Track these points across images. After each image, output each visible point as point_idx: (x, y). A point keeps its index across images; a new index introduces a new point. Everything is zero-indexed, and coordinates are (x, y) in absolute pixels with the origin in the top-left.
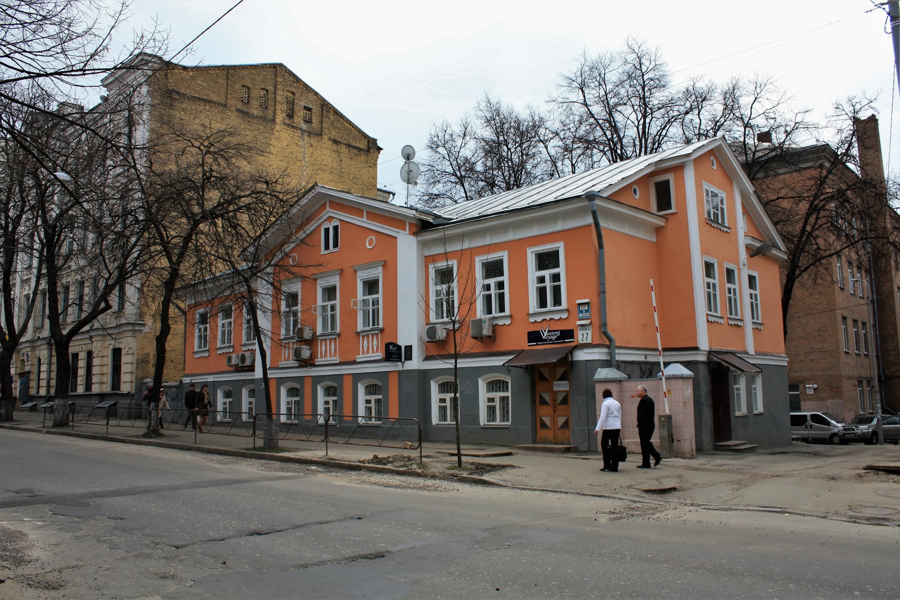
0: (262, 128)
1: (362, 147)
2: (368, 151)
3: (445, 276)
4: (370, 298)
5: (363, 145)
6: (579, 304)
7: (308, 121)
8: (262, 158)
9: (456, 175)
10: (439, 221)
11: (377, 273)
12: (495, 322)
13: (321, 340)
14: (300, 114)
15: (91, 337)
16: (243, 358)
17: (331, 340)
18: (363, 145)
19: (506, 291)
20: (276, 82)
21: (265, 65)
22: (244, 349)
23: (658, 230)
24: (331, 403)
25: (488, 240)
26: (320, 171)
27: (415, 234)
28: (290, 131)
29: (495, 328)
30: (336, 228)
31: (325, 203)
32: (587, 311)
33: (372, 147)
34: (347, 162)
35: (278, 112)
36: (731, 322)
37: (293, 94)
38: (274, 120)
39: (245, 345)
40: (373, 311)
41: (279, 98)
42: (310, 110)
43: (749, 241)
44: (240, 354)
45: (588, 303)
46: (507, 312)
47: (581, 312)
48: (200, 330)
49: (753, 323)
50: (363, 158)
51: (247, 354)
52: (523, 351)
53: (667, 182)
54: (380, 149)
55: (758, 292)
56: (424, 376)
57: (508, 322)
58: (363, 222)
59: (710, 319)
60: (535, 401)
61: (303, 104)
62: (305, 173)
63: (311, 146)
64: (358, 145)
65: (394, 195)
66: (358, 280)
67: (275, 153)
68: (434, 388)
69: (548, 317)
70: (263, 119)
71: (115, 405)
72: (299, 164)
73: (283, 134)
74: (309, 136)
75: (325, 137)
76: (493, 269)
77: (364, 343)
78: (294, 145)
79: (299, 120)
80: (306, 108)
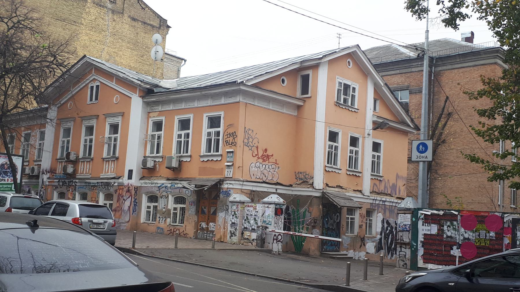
1: (155, 24)
2: (159, 28)
3: (158, 126)
4: (157, 133)
5: (156, 23)
6: (228, 152)
11: (118, 120)
12: (182, 159)
13: (82, 162)
16: (33, 169)
17: (87, 162)
18: (156, 23)
19: (190, 139)
22: (35, 163)
23: (299, 107)
25: (183, 106)
26: (120, 40)
27: (142, 97)
29: (180, 162)
30: (97, 87)
31: (92, 69)
32: (231, 157)
36: (348, 173)
39: (36, 161)
43: (375, 119)
44: (31, 167)
45: (232, 152)
46: (161, 154)
49: (371, 175)
51: (36, 167)
53: (308, 76)
54: (169, 27)
57: (188, 159)
58: (113, 85)
59: (327, 169)
60: (198, 212)
63: (114, 20)
64: (152, 23)
65: (185, 61)
66: (107, 123)
69: (210, 159)
75: (125, 15)
76: (185, 124)
77: (106, 166)
78: (100, 20)
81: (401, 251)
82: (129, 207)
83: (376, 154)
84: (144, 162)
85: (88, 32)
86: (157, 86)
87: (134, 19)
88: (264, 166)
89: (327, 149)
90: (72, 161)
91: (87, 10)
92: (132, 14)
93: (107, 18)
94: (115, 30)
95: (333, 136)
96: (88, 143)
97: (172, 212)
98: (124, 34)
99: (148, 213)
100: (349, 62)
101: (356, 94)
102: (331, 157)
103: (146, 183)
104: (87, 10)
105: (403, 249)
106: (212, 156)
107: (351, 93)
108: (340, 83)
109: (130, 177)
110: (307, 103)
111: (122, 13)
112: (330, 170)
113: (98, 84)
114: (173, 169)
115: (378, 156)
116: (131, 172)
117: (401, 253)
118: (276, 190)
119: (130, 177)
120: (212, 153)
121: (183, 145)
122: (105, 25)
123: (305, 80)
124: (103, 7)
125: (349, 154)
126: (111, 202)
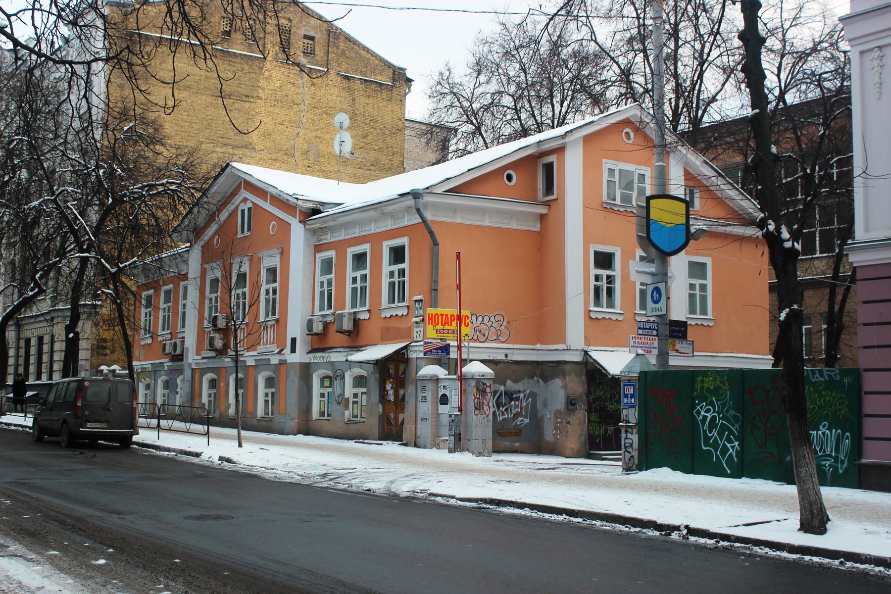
0: (246, 67)
6: (416, 301)
8: (247, 105)
9: (472, 123)
14: (298, 46)
15: (52, 319)
23: (542, 217)
26: (324, 116)
30: (250, 209)
32: (421, 308)
33: (400, 79)
34: (362, 100)
37: (290, 20)
40: (361, 288)
42: (312, 38)
45: (421, 300)
48: (211, 299)
50: (385, 94)
54: (409, 81)
55: (709, 282)
56: (306, 370)
58: (266, 206)
59: (593, 315)
61: (302, 32)
62: (304, 120)
67: (264, 97)
71: (406, 347)
73: (274, 73)
78: (290, 86)
80: (306, 37)
81: (626, 438)
83: (697, 282)
84: (310, 323)
85: (270, 109)
88: (480, 319)
89: (593, 282)
90: (221, 329)
91: (267, 74)
93: (300, 81)
94: (316, 100)
95: (604, 260)
96: (326, 288)
97: (351, 400)
98: (331, 104)
99: (266, 402)
100: (627, 133)
103: (319, 357)
104: (267, 73)
105: (629, 435)
108: (611, 171)
109: (293, 350)
110: (552, 208)
112: (600, 316)
113: (251, 205)
114: (349, 333)
115: (700, 285)
116: (294, 340)
117: (627, 441)
118: (506, 356)
119: (293, 350)
121: (359, 295)
122: (298, 94)
126: (273, 390)
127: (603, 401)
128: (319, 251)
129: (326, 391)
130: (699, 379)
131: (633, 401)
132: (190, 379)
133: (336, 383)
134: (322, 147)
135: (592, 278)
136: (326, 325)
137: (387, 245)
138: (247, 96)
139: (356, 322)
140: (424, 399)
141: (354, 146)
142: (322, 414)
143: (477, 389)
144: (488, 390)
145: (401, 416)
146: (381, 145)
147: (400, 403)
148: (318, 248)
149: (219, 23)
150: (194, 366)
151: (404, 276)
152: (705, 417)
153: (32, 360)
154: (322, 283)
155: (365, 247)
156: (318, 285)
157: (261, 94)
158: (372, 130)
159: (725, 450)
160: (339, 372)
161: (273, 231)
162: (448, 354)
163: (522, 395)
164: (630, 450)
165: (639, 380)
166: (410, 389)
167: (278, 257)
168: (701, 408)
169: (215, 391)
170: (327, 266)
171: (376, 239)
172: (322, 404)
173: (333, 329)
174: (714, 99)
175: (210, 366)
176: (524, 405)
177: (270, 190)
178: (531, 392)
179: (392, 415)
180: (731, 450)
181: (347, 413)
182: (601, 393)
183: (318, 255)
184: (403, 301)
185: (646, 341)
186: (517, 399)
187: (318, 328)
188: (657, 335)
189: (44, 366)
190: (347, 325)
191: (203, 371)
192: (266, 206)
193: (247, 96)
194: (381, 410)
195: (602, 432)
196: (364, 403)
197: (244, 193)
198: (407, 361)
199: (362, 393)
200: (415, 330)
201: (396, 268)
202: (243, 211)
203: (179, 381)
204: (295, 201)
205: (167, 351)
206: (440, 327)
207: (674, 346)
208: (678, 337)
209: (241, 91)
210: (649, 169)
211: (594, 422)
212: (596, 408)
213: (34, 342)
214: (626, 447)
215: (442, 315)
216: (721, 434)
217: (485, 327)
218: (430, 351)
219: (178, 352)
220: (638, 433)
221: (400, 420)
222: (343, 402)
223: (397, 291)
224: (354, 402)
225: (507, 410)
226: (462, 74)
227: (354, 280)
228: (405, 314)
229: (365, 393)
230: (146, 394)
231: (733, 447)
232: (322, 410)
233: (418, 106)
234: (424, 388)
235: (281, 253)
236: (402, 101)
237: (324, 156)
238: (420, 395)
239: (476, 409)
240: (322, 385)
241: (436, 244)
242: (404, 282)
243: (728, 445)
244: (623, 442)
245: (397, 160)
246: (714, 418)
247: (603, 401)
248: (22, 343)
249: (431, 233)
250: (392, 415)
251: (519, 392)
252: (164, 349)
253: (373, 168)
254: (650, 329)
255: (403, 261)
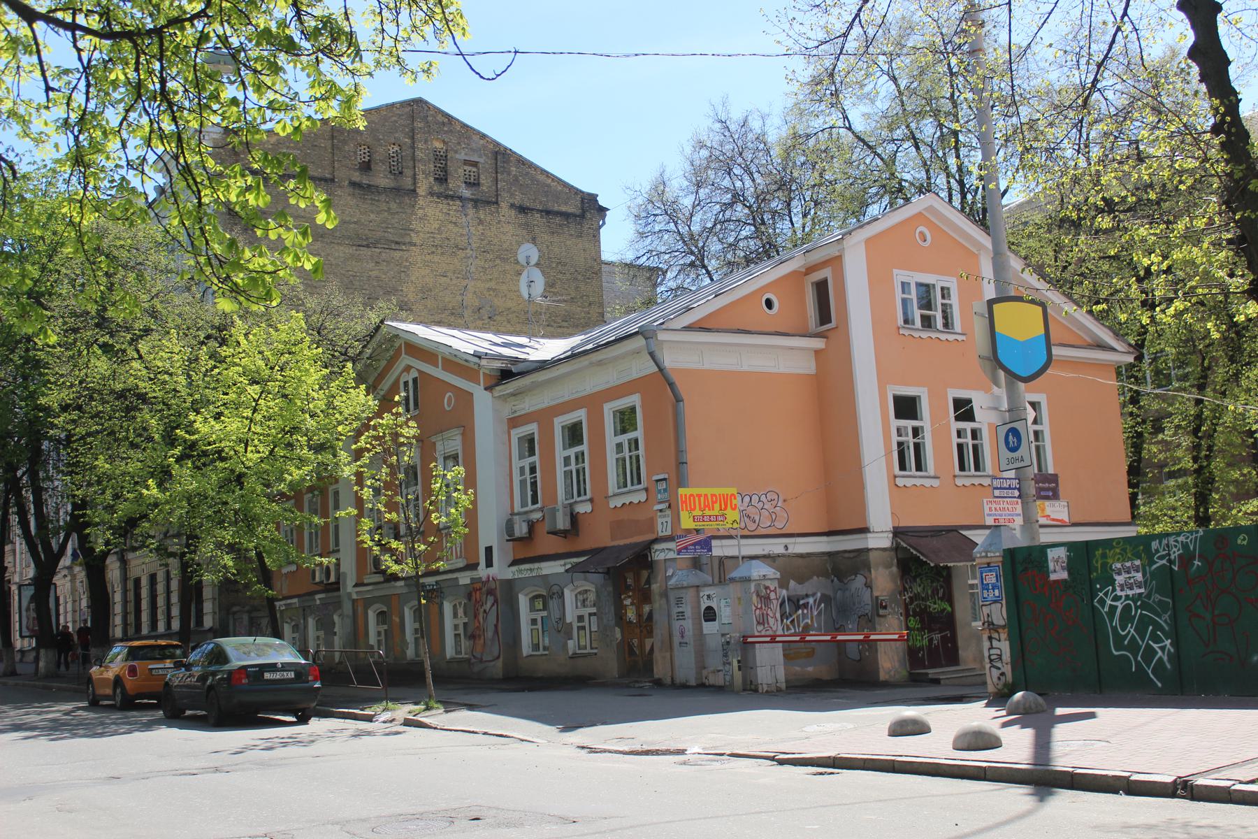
0: (393, 206)
2: (582, 216)
7: (473, 184)
8: (397, 254)
10: (520, 367)
20: (413, 130)
21: (393, 105)
24: (461, 627)
26: (498, 261)
27: (488, 388)
28: (443, 206)
30: (415, 380)
32: (665, 490)
33: (589, 210)
35: (420, 176)
38: (414, 191)
40: (578, 471)
41: (419, 154)
42: (475, 164)
47: (659, 491)
52: (604, 548)
54: (603, 210)
62: (473, 269)
63: (481, 222)
64: (564, 209)
68: (523, 602)
70: (397, 191)
72: (461, 254)
73: (430, 211)
74: (475, 207)
78: (451, 226)
79: (457, 184)
80: (466, 162)
81: (992, 648)
82: (496, 626)
86: (516, 361)
87: (523, 210)
88: (747, 499)
92: (518, 200)
95: (906, 407)
96: (626, 454)
98: (505, 246)
101: (954, 301)
102: (909, 457)
103: (525, 571)
104: (421, 211)
105: (995, 643)
106: (629, 492)
107: (939, 300)
109: (489, 564)
111: (492, 202)
113: (415, 374)
114: (564, 534)
116: (489, 550)
117: (992, 652)
119: (489, 564)
120: (629, 487)
121: (577, 481)
122: (462, 235)
123: (821, 288)
124: (452, 197)
125: (955, 440)
127: (923, 599)
128: (515, 427)
129: (538, 616)
130: (1099, 552)
131: (997, 592)
132: (350, 612)
133: (553, 604)
134: (498, 302)
135: (894, 432)
136: (532, 526)
137: (609, 409)
138: (397, 243)
139: (574, 518)
140: (681, 615)
141: (550, 285)
142: (536, 647)
143: (758, 595)
144: (773, 596)
145: (648, 643)
146: (573, 295)
147: (646, 624)
148: (514, 422)
149: (355, 153)
150: (355, 597)
151: (637, 448)
152: (1113, 609)
153: (145, 605)
154: (522, 469)
155: (580, 415)
156: (516, 473)
157: (415, 239)
158: (560, 276)
159: (1150, 652)
160: (555, 589)
161: (449, 404)
162: (710, 550)
163: (811, 600)
164: (999, 665)
165: (1003, 563)
166: (658, 603)
167: (459, 438)
168: (1106, 594)
169: (386, 627)
170: (529, 444)
171: (593, 402)
172: (535, 633)
173: (542, 530)
174: (1005, 192)
175: (377, 594)
176: (815, 613)
177: (442, 349)
178: (823, 595)
179: (635, 641)
180: (1160, 653)
181: (571, 644)
182: (919, 590)
183: (513, 432)
184: (639, 482)
185: (1006, 506)
186: (806, 606)
187: (521, 529)
188: (1020, 497)
189: (159, 611)
190: (562, 523)
191: (368, 603)
192: (438, 372)
193: (397, 243)
194: (618, 635)
195: (925, 642)
196: (594, 628)
197: (406, 360)
198: (650, 565)
199: (590, 615)
200: (660, 521)
201: (572, 452)
202: (406, 383)
203: (336, 618)
204: (476, 360)
205: (317, 579)
206: (697, 512)
207: (1043, 510)
208: (1047, 498)
209: (391, 237)
210: (954, 280)
211: (914, 629)
212: (914, 610)
213: (144, 582)
214: (991, 661)
215: (699, 496)
216: (1141, 631)
217: (754, 510)
218: (686, 548)
219: (332, 579)
220: (1010, 638)
221: (648, 648)
222: (564, 630)
223: (631, 473)
224: (579, 628)
225: (792, 622)
226: (678, 184)
227: (567, 460)
228: (643, 500)
229: (595, 614)
230: (318, 638)
231: (1163, 649)
232: (535, 641)
233: (617, 241)
234: (679, 601)
235: (463, 434)
236: (596, 238)
237: (500, 313)
238: (675, 610)
239: (759, 623)
240: (532, 609)
241: (678, 399)
242: (638, 457)
243: (1155, 646)
244: (986, 654)
245: (594, 310)
246: (1127, 608)
247: (923, 599)
248: (130, 585)
249: (671, 385)
250: (635, 641)
251: (807, 596)
252: (314, 578)
253: (565, 324)
254: (1010, 488)
255: (580, 442)
